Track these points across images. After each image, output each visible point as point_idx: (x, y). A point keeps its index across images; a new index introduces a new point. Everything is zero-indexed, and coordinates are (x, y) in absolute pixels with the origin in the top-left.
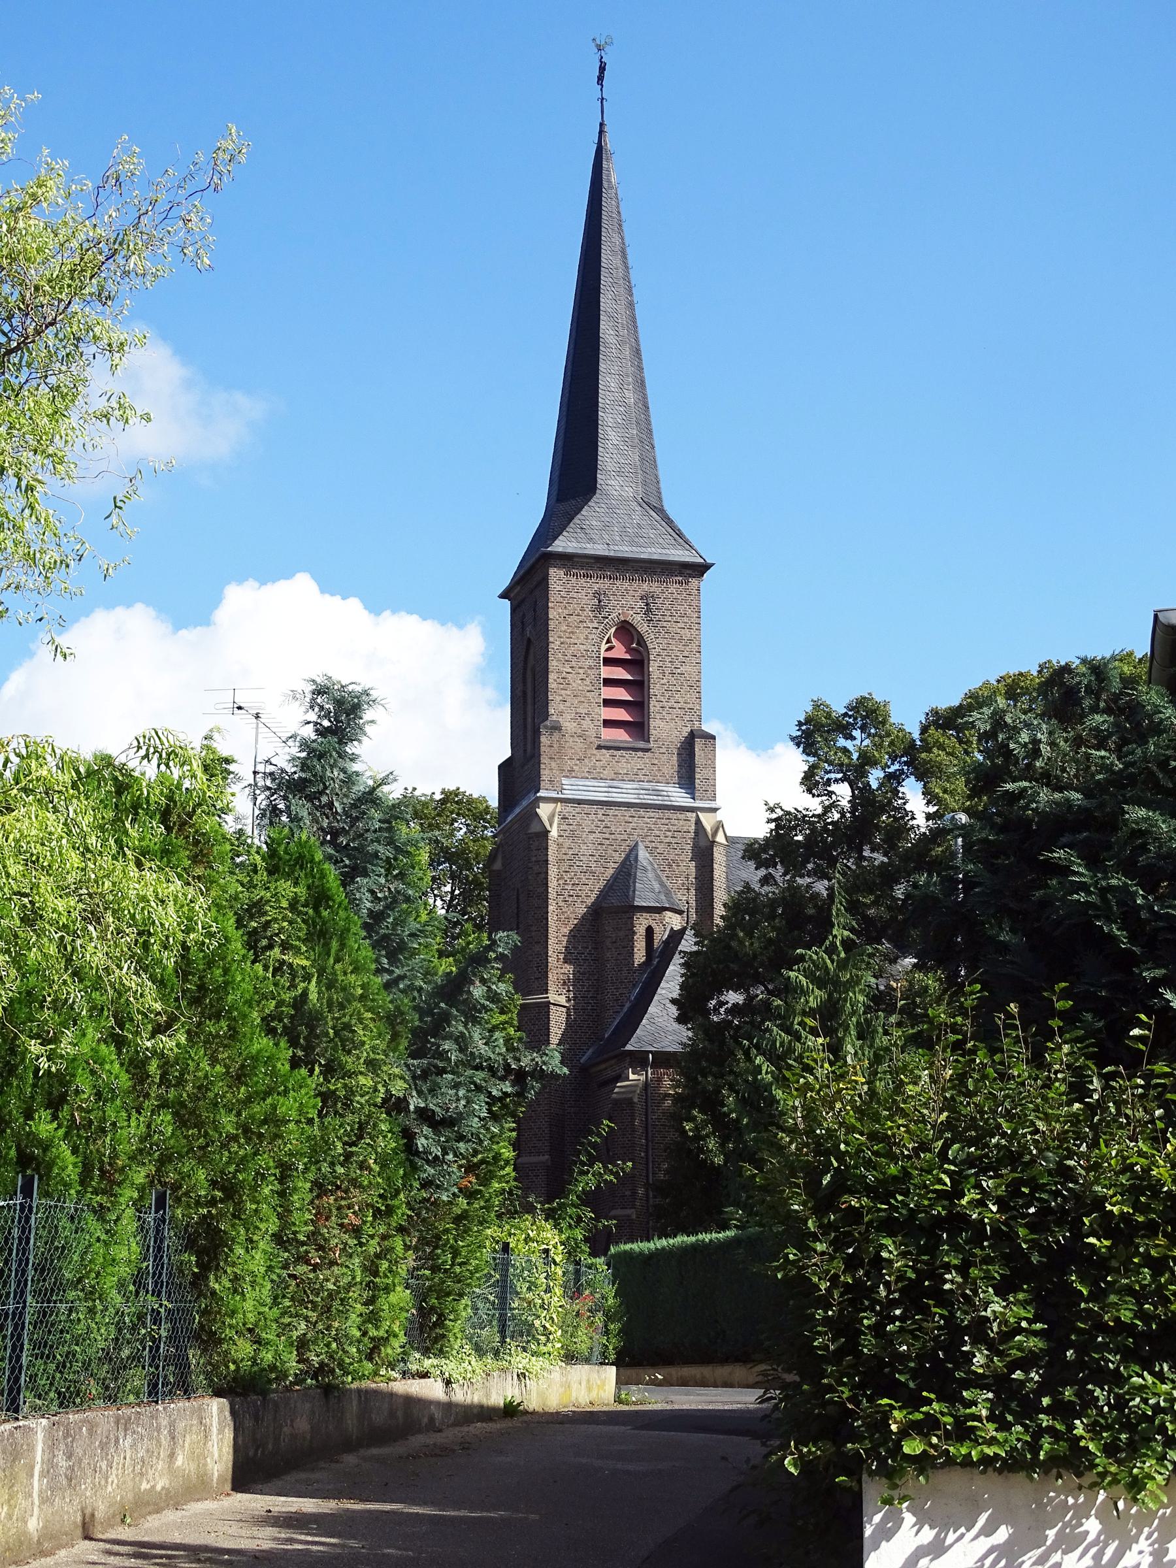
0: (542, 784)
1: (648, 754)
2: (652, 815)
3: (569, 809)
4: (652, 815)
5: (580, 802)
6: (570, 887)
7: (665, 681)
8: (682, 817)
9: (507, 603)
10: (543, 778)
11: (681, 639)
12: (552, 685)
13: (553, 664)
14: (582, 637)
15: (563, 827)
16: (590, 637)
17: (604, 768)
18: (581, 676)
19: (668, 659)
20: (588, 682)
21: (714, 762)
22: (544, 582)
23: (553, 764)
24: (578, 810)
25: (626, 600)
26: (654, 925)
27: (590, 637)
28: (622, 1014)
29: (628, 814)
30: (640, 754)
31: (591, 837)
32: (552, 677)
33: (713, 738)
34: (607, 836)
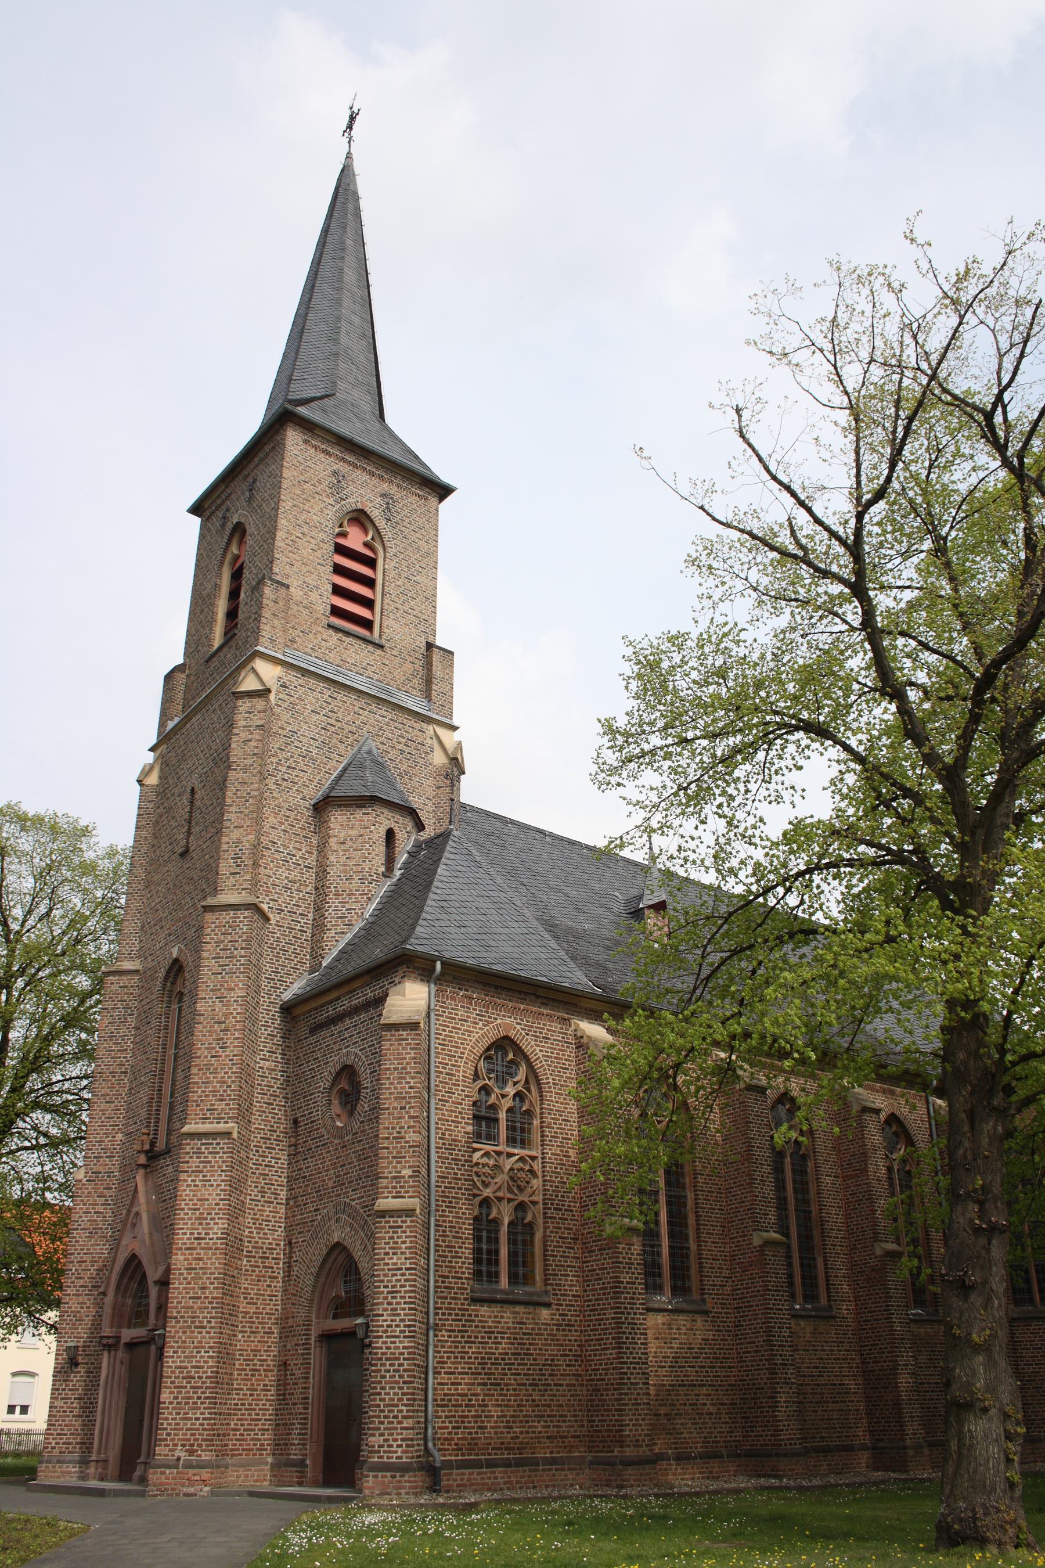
0: (261, 640)
1: (379, 652)
2: (385, 713)
3: (291, 677)
4: (385, 713)
5: (304, 672)
6: (284, 769)
7: (399, 583)
8: (417, 726)
9: (196, 521)
10: (264, 633)
11: (418, 549)
12: (279, 543)
13: (282, 522)
14: (317, 508)
15: (281, 696)
16: (326, 512)
17: (331, 650)
18: (313, 546)
19: (405, 563)
20: (319, 554)
21: (451, 678)
22: (279, 448)
23: (276, 622)
24: (301, 681)
25: (366, 490)
26: (396, 830)
27: (326, 512)
28: (349, 936)
29: (358, 704)
30: (370, 648)
31: (315, 717)
32: (280, 535)
33: (452, 653)
34: (333, 722)
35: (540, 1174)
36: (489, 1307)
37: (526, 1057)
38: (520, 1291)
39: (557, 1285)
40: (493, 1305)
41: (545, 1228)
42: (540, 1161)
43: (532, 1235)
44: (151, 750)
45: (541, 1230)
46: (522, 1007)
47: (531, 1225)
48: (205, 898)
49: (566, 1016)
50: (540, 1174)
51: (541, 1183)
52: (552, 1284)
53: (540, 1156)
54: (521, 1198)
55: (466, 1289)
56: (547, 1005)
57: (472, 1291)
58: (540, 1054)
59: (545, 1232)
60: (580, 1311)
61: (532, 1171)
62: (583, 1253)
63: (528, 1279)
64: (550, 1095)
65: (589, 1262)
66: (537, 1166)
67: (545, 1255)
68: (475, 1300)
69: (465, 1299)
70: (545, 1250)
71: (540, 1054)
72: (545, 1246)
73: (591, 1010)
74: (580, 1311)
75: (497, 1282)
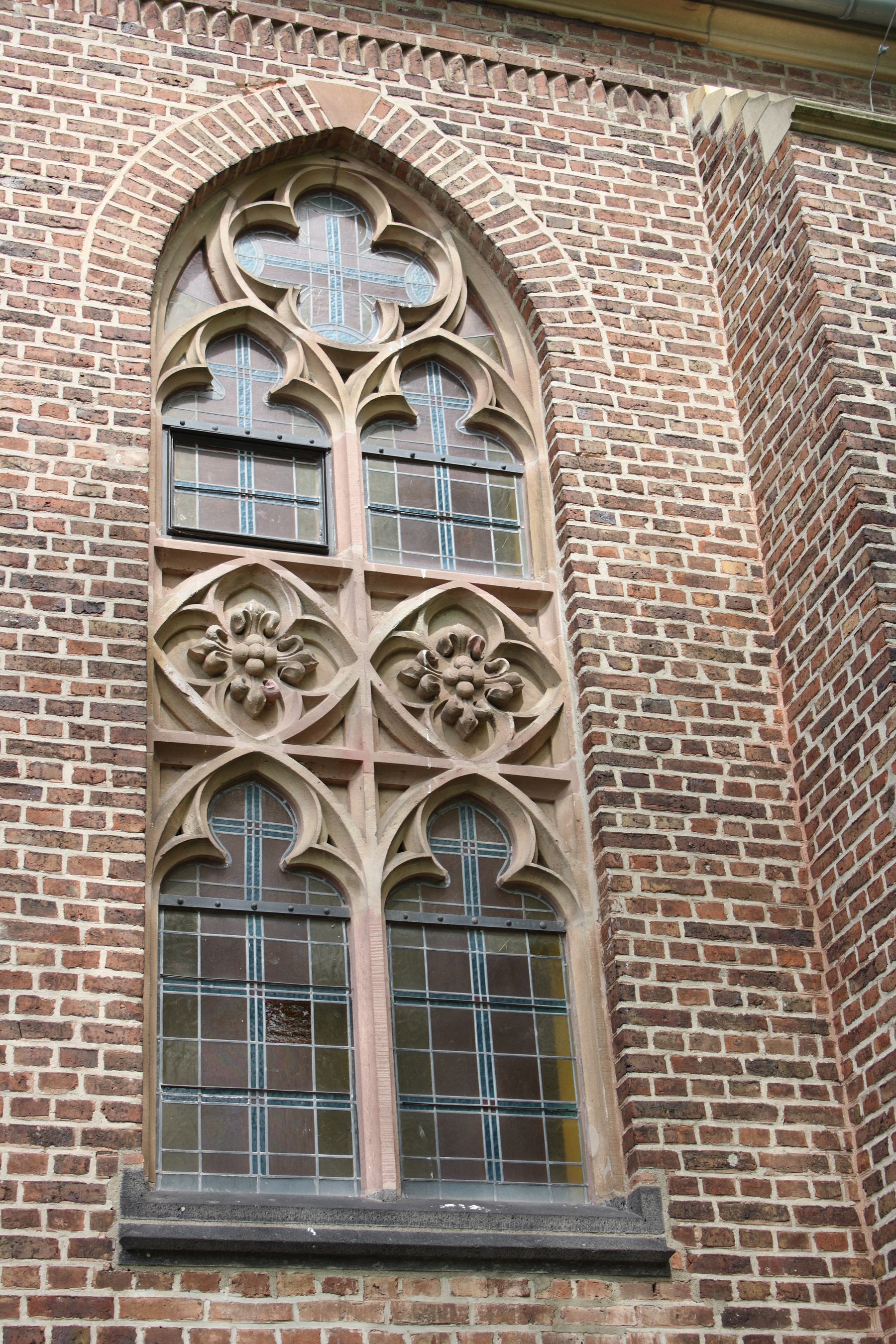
35: (563, 662)
36: (245, 1287)
37: (451, 212)
38: (486, 1204)
39: (694, 1160)
40: (275, 1276)
41: (607, 889)
42: (560, 604)
43: (550, 939)
44: (292, 233)
45: (593, 903)
46: (419, 40)
47: (533, 890)
48: (139, 1029)
49: (650, 82)
50: (563, 662)
51: (574, 700)
52: (668, 1161)
53: (558, 586)
54: (458, 765)
55: (96, 1194)
56: (547, 38)
57: (129, 1205)
58: (524, 201)
59: (605, 907)
60: (861, 1294)
61: (518, 654)
62: (839, 997)
63: (540, 1146)
64: (591, 345)
65: (868, 1028)
66: (548, 635)
67: (618, 1018)
68: (146, 1252)
69: (80, 1249)
70: (618, 993)
71: (524, 201)
72: (613, 971)
73: (776, 68)
74: (861, 1294)
75: (346, 1168)
